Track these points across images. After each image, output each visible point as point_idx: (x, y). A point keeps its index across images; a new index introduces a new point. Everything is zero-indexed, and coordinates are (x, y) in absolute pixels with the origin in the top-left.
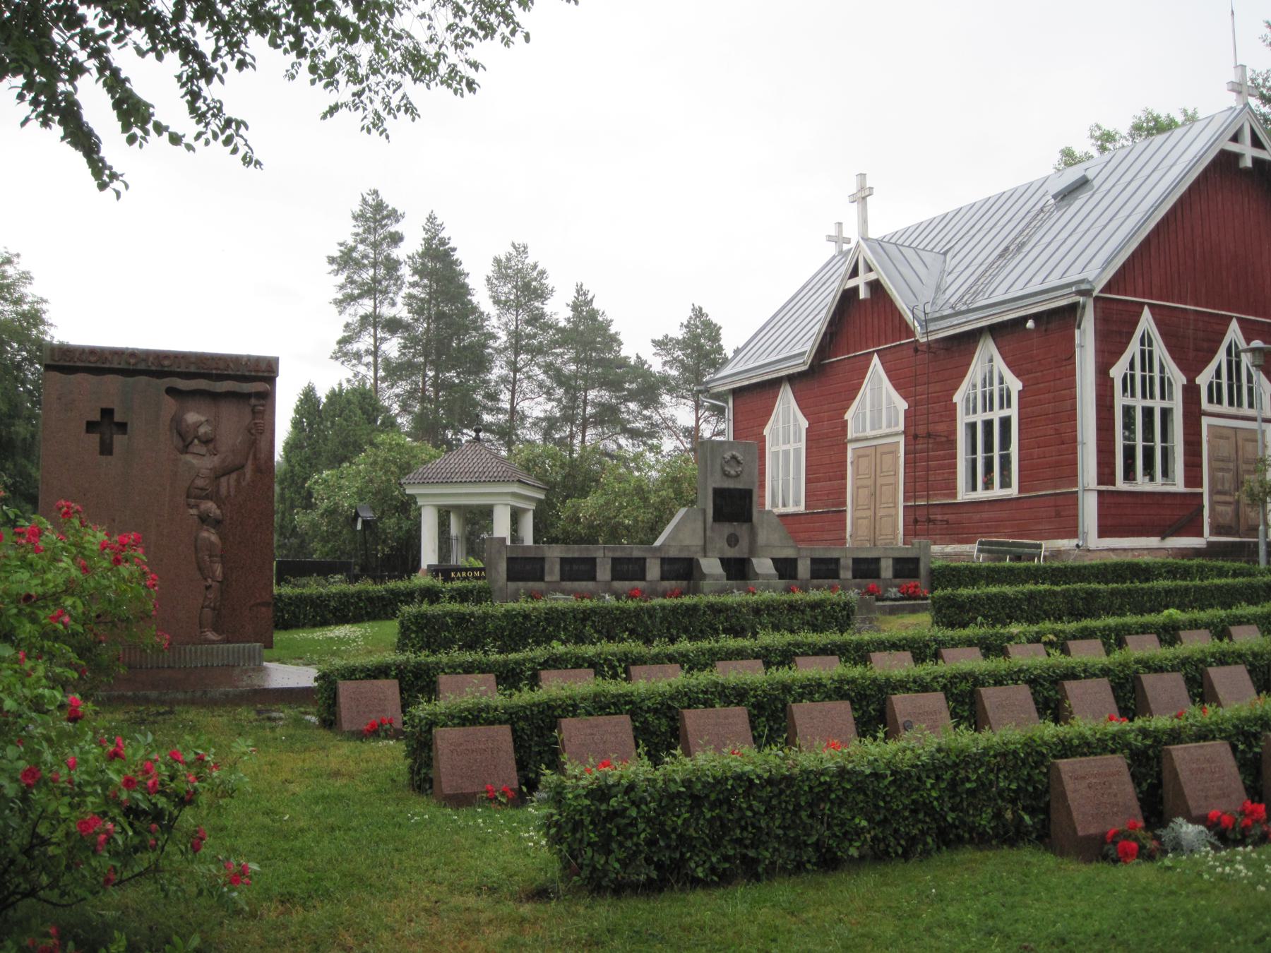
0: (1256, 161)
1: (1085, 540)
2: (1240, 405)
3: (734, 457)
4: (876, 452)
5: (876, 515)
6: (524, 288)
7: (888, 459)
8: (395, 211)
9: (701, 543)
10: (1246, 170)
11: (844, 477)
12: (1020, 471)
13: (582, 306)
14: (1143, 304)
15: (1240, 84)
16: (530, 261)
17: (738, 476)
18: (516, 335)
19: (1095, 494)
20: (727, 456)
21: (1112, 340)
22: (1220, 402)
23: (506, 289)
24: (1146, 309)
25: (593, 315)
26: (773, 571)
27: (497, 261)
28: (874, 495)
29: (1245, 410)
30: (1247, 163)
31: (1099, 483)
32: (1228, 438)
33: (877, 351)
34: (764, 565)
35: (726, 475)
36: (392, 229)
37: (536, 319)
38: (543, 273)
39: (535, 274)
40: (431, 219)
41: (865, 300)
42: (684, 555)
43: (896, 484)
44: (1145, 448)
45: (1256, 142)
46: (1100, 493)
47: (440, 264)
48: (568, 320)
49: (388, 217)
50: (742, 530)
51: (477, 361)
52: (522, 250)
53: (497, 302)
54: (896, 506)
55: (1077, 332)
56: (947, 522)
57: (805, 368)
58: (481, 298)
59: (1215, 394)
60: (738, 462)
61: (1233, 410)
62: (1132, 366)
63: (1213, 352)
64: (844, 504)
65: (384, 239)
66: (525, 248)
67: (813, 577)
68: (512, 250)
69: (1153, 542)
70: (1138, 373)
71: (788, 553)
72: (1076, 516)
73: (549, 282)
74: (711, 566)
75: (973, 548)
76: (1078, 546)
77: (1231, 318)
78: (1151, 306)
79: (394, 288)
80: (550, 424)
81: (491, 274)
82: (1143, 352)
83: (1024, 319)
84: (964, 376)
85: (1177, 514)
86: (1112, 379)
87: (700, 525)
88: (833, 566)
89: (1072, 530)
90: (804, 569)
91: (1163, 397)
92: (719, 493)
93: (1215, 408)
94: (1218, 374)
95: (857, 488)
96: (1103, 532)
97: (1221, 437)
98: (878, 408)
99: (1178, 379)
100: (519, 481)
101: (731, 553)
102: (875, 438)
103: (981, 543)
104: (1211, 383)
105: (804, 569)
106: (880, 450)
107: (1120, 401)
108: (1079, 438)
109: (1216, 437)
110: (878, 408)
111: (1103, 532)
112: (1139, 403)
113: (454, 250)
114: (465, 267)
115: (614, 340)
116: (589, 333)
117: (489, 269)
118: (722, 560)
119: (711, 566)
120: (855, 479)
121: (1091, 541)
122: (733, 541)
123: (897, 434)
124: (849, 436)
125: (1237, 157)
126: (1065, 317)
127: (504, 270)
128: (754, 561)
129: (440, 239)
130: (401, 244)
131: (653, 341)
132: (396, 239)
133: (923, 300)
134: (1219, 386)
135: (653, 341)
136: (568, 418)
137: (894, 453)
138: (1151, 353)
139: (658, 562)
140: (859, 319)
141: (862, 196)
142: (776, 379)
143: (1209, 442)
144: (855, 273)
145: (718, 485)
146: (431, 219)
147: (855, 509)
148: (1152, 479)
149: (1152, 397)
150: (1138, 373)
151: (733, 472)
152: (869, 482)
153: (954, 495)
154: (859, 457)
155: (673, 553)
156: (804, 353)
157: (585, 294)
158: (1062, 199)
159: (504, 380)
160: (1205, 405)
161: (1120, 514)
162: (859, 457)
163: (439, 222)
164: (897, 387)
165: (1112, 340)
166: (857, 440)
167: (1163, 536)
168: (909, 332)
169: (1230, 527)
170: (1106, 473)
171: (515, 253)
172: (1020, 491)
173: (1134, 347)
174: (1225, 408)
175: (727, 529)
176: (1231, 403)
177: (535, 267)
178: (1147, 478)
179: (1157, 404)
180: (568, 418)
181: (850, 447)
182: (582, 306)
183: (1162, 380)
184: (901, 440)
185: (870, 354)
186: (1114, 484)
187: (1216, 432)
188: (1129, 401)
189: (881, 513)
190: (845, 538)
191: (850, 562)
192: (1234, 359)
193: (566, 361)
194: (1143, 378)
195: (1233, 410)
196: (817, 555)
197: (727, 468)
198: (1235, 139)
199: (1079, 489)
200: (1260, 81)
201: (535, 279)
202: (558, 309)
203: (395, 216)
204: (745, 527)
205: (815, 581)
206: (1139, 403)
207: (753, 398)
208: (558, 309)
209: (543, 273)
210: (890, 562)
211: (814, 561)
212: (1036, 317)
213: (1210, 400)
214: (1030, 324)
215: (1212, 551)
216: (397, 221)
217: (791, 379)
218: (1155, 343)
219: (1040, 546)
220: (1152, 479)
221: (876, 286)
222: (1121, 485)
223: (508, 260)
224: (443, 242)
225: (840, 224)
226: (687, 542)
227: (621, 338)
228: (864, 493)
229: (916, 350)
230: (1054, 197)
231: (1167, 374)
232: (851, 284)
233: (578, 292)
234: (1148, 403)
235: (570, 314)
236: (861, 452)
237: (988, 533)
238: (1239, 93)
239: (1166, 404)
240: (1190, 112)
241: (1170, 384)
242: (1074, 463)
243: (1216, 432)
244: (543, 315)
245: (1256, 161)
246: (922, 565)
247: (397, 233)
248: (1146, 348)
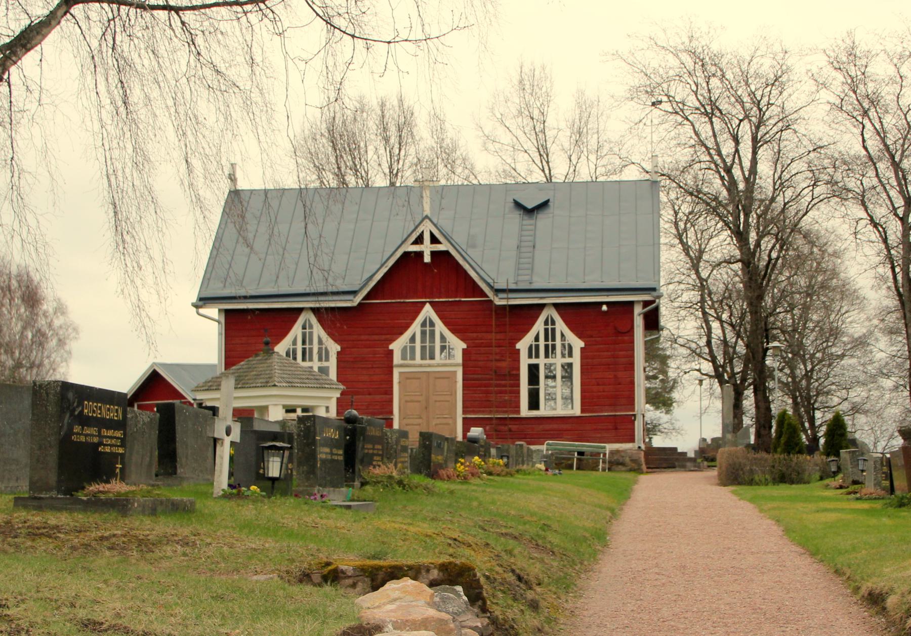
25: (62, 304)
62: (537, 339)
82: (546, 330)
94: (537, 339)
97: (407, 378)
125: (420, 254)
134: (537, 347)
138: (553, 330)
188: (534, 361)
195: (428, 362)
214: (605, 308)
218: (557, 323)
248: (550, 327)
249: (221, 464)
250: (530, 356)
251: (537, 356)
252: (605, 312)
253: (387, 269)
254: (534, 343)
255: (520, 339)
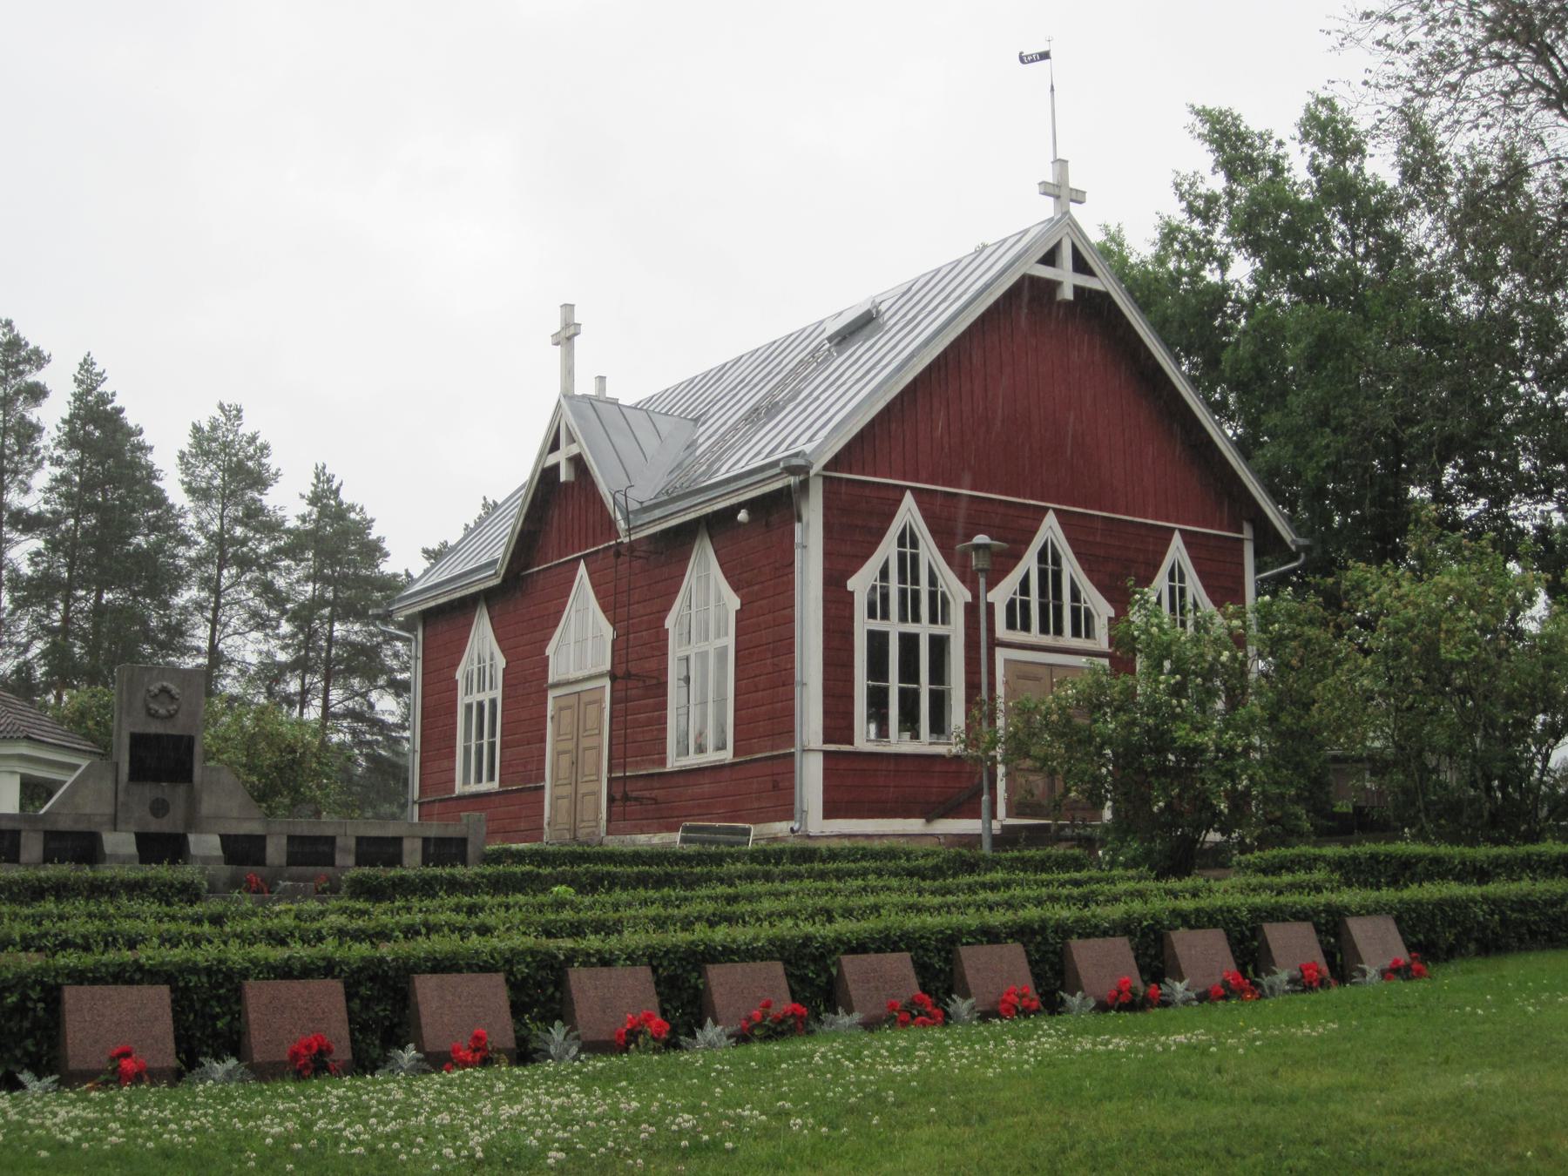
0: (1078, 290)
1: (803, 821)
2: (1059, 631)
3: (164, 690)
4: (580, 702)
5: (575, 794)
6: (235, 469)
7: (592, 709)
8: (37, 352)
9: (109, 810)
10: (1067, 303)
11: (543, 740)
12: (736, 725)
13: (324, 496)
14: (903, 489)
15: (1058, 186)
16: (246, 429)
17: (171, 716)
18: (220, 540)
19: (820, 757)
20: (154, 688)
21: (852, 535)
22: (1026, 627)
23: (207, 472)
24: (908, 495)
25: (340, 513)
26: (220, 853)
27: (197, 429)
28: (574, 763)
29: (1067, 639)
30: (1067, 294)
31: (825, 742)
32: (1037, 679)
33: (584, 557)
34: (205, 844)
35: (152, 715)
36: (30, 379)
37: (255, 517)
38: (264, 448)
39: (251, 450)
40: (87, 364)
41: (566, 483)
42: (82, 827)
43: (599, 748)
44: (902, 692)
45: (1081, 265)
46: (826, 754)
47: (101, 432)
48: (303, 519)
49: (28, 360)
50: (175, 794)
51: (156, 577)
52: (234, 414)
53: (191, 490)
54: (599, 780)
55: (798, 526)
56: (655, 801)
57: (496, 581)
58: (172, 487)
59: (1018, 615)
60: (172, 698)
61: (1049, 640)
62: (884, 574)
63: (1018, 557)
64: (543, 779)
65: (18, 393)
66: (239, 411)
67: (289, 864)
68: (218, 413)
69: (915, 825)
70: (894, 586)
71: (254, 828)
72: (793, 787)
73: (273, 462)
74: (120, 842)
75: (677, 837)
76: (792, 830)
77: (1046, 509)
78: (914, 490)
79: (29, 467)
80: (271, 674)
81: (186, 449)
82: (902, 557)
83: (734, 510)
84: (677, 592)
85: (947, 787)
86: (852, 594)
87: (108, 785)
88: (326, 849)
89: (786, 807)
90: (276, 851)
91: (933, 620)
92: (139, 742)
93: (1018, 636)
94: (884, 574)
95: (558, 754)
96: (830, 812)
97: (1026, 677)
98: (582, 640)
99: (958, 594)
100: (28, 738)
101: (155, 826)
102: (577, 682)
103: (687, 830)
104: (874, 588)
105: (276, 851)
106: (585, 698)
107: (862, 626)
108: (798, 677)
109: (1019, 677)
110: (582, 640)
111: (830, 812)
112: (894, 628)
113: (121, 410)
114: (147, 438)
115: (374, 551)
116: (338, 538)
117: (185, 442)
118: (138, 835)
119: (120, 842)
120: (556, 742)
121: (814, 820)
122: (159, 808)
123: (600, 676)
124: (550, 680)
125: (1053, 285)
126: (776, 508)
127: (206, 443)
128: (192, 838)
129: (101, 395)
130: (45, 403)
131: (425, 551)
132: (37, 393)
133: (632, 485)
134: (1025, 606)
135: (425, 551)
136: (301, 665)
137: (600, 701)
138: (915, 558)
139: (41, 836)
140: (559, 506)
141: (567, 337)
142: (462, 600)
143: (1006, 683)
144: (555, 446)
145: (139, 729)
146: (87, 364)
147: (555, 786)
148: (916, 736)
149: (885, 616)
150: (894, 586)
151: (162, 711)
152: (570, 745)
153: (663, 762)
154: (561, 709)
155: (64, 824)
156: (495, 562)
157: (329, 481)
158: (839, 344)
159: (200, 607)
160: (1001, 631)
161: (855, 783)
162: (561, 709)
163: (98, 369)
164: (605, 610)
165: (852, 535)
166: (557, 685)
167: (929, 817)
168: (610, 527)
169: (1040, 805)
170: (838, 723)
171: (223, 419)
172: (735, 755)
173: (888, 548)
174: (1035, 636)
175: (149, 791)
176: (1044, 629)
177: (252, 440)
178: (907, 735)
179: (924, 630)
180: (301, 665)
181: (551, 694)
182: (324, 496)
183: (933, 596)
184: (607, 683)
185: (577, 560)
186: (852, 743)
187: (1019, 672)
188: (878, 625)
189: (583, 789)
190: (542, 828)
191: (352, 843)
192: (1050, 567)
193: (296, 581)
194: (903, 593)
195: (1049, 640)
196: (298, 831)
197: (154, 706)
198: (1050, 258)
199: (796, 749)
200: (1186, 186)
201: (251, 458)
202: (287, 501)
203: (38, 359)
204: (182, 789)
205: (295, 870)
206: (894, 628)
207: (444, 621)
208: (287, 501)
209: (264, 448)
210: (418, 844)
211: (291, 839)
212: (749, 505)
213: (1011, 625)
214: (743, 516)
215: (1007, 839)
216: (39, 367)
217: (488, 597)
218: (921, 543)
219: (747, 832)
220: (916, 736)
221: (578, 462)
222: (864, 738)
223: (214, 428)
224: (104, 399)
225: (602, 379)
226: (88, 811)
227: (386, 546)
228: (565, 760)
229: (618, 554)
230: (830, 339)
231: (942, 587)
232: (551, 460)
233: (317, 477)
234: (910, 628)
235: (304, 508)
236: (563, 703)
237: (700, 817)
238: (1057, 197)
239: (939, 630)
240: (1113, 229)
241: (945, 602)
242: (789, 713)
243: (1019, 672)
244: (262, 510)
245: (1078, 290)
246: (470, 849)
247: (37, 385)
248: (908, 550)
249: (868, 836)
250: (872, 614)
251: (885, 616)
252: (741, 524)
253: (940, 349)
254: (1018, 597)
255: (854, 572)
